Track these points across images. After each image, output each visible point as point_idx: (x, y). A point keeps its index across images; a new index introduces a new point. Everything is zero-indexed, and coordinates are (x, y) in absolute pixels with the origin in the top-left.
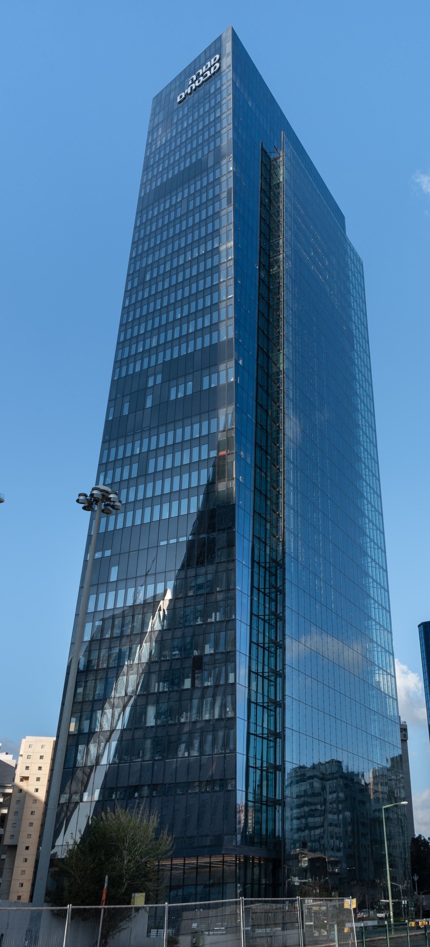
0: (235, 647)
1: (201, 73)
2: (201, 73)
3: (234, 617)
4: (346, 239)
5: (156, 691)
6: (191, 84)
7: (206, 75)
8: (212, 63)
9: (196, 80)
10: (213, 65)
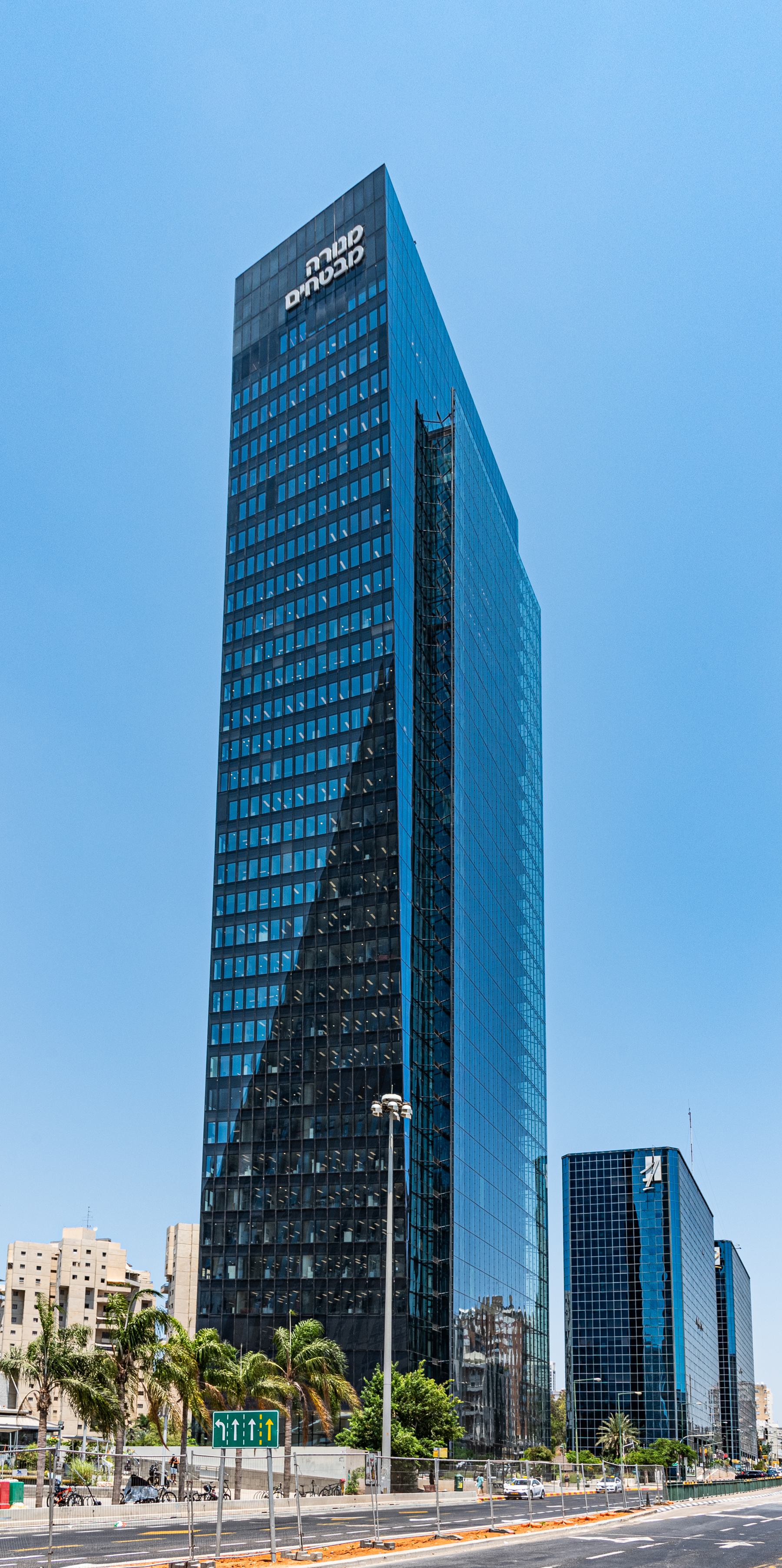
0: (397, 818)
1: (329, 259)
2: (329, 259)
3: (396, 888)
4: (518, 562)
5: (314, 738)
6: (311, 277)
7: (340, 266)
8: (350, 244)
9: (319, 271)
10: (352, 248)
